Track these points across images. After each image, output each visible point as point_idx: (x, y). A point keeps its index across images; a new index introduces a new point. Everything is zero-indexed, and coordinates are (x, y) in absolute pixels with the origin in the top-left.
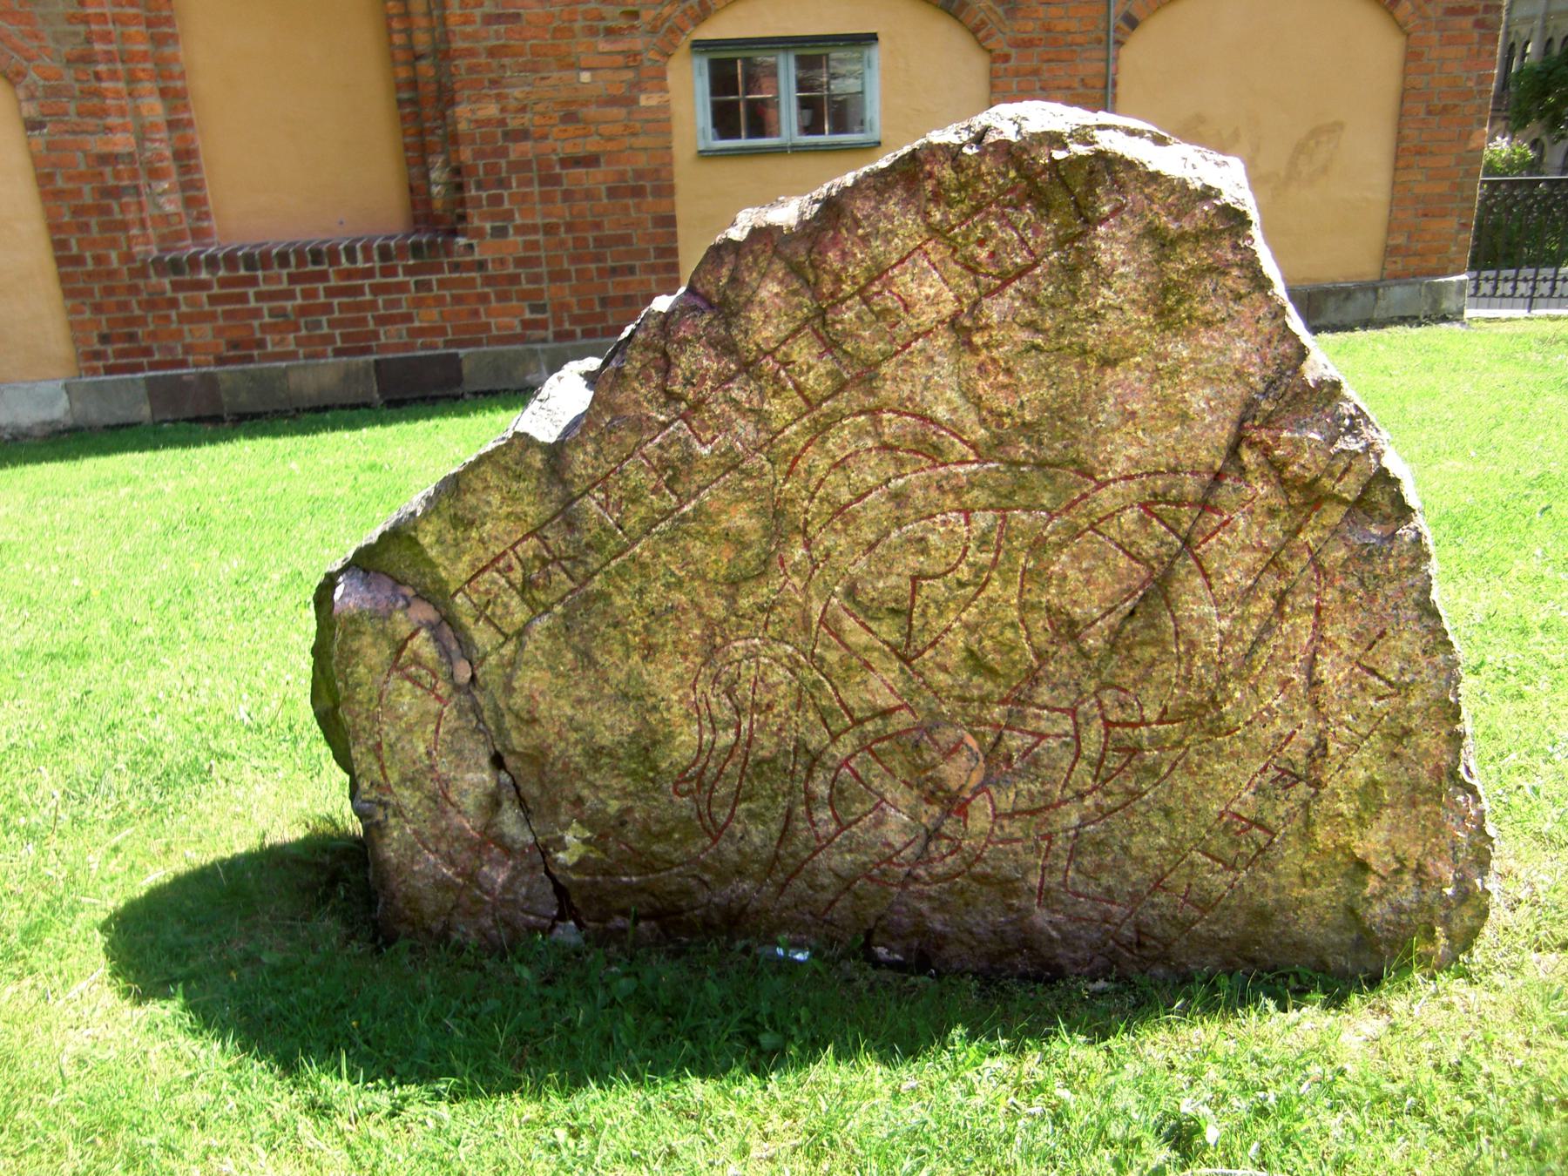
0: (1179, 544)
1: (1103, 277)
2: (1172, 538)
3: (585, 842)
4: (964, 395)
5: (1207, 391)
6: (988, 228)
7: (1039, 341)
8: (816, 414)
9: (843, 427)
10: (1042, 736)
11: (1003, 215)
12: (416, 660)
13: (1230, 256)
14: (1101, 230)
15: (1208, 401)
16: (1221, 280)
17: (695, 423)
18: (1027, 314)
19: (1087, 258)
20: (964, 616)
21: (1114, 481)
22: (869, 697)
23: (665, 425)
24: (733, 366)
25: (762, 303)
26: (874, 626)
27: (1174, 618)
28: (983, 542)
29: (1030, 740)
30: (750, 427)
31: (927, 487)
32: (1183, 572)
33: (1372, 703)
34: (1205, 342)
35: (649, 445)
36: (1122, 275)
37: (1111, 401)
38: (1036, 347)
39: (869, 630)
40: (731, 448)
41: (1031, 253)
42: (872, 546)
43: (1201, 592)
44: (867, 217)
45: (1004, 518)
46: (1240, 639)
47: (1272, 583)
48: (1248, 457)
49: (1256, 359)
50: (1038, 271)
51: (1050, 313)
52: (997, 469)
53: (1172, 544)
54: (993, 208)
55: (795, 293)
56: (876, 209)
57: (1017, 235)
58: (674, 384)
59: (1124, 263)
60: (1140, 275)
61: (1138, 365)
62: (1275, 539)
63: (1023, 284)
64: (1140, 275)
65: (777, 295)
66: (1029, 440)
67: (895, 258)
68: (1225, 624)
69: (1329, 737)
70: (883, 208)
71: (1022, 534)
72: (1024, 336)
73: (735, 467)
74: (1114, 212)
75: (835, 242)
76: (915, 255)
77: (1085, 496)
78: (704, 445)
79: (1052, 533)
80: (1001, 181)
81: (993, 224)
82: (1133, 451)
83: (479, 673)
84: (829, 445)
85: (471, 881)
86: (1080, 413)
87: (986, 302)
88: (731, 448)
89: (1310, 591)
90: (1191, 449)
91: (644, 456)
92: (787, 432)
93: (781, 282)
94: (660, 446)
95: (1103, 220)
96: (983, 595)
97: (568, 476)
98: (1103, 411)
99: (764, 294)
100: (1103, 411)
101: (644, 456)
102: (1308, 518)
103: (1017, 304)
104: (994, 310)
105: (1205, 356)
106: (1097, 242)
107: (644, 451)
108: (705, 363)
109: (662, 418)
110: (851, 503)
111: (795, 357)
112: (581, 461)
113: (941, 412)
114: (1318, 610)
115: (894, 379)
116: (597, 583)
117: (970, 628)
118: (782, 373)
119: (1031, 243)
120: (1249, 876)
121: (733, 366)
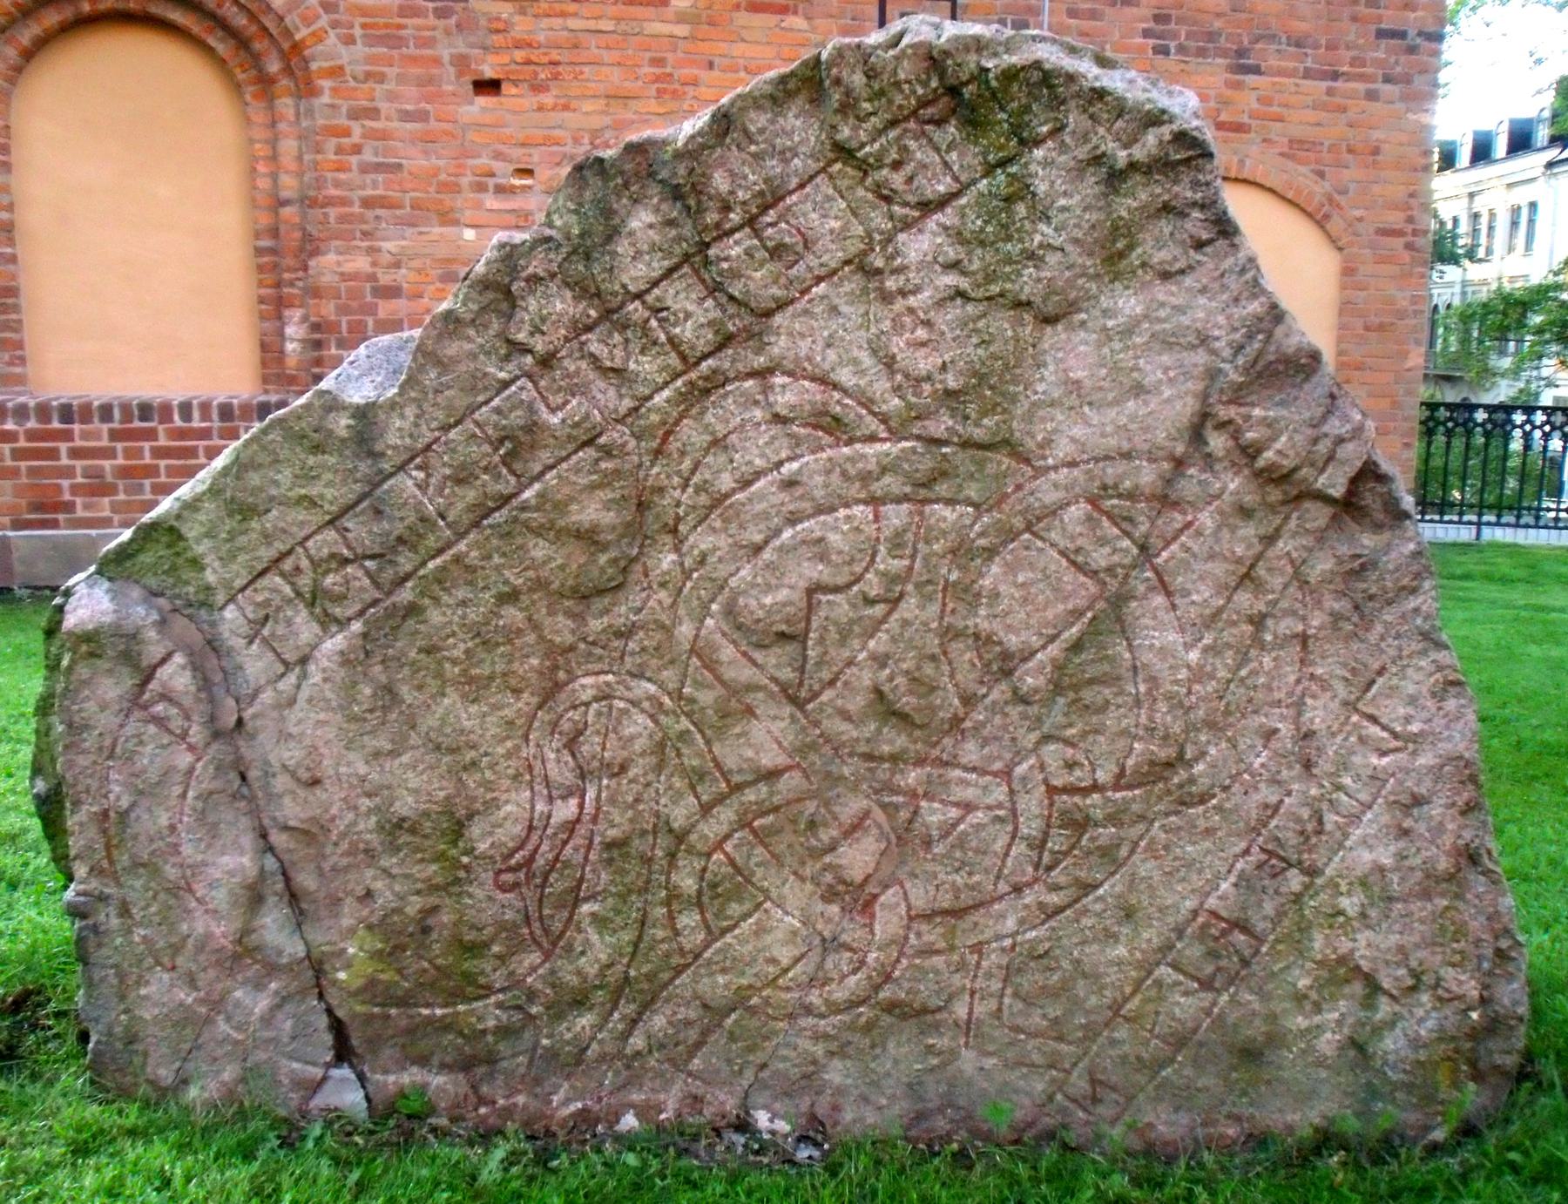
0: (1135, 551)
2: (1126, 543)
4: (874, 352)
7: (964, 283)
8: (693, 375)
10: (968, 807)
12: (165, 697)
13: (1189, 194)
14: (1039, 153)
15: (1166, 370)
18: (951, 253)
19: (1021, 191)
20: (872, 644)
22: (750, 753)
23: (506, 384)
24: (593, 313)
25: (631, 234)
26: (758, 656)
29: (954, 813)
30: (612, 393)
31: (828, 472)
33: (1374, 760)
37: (1051, 368)
39: (754, 663)
40: (587, 416)
42: (758, 549)
44: (762, 131)
45: (921, 513)
48: (1217, 442)
49: (1221, 319)
50: (963, 201)
52: (914, 450)
53: (1126, 551)
55: (671, 223)
56: (772, 122)
57: (941, 160)
60: (1085, 209)
61: (1083, 323)
62: (1249, 547)
63: (947, 217)
64: (1085, 209)
65: (651, 226)
66: (953, 412)
68: (1194, 656)
70: (781, 120)
72: (951, 279)
74: (1054, 133)
75: (722, 163)
76: (818, 180)
77: (1019, 487)
78: (553, 410)
79: (982, 534)
80: (920, 91)
81: (912, 144)
82: (1078, 431)
83: (247, 714)
84: (709, 418)
86: (1015, 381)
87: (902, 237)
88: (587, 416)
91: (477, 423)
92: (657, 399)
93: (657, 210)
94: (498, 411)
95: (1038, 143)
97: (379, 447)
98: (1042, 379)
99: (634, 224)
100: (1042, 379)
101: (477, 423)
104: (918, 246)
105: (1162, 313)
106: (1033, 168)
107: (476, 416)
108: (559, 306)
109: (502, 375)
110: (734, 491)
111: (669, 303)
112: (395, 434)
113: (845, 376)
115: (790, 334)
117: (880, 660)
118: (654, 323)
121: (593, 313)
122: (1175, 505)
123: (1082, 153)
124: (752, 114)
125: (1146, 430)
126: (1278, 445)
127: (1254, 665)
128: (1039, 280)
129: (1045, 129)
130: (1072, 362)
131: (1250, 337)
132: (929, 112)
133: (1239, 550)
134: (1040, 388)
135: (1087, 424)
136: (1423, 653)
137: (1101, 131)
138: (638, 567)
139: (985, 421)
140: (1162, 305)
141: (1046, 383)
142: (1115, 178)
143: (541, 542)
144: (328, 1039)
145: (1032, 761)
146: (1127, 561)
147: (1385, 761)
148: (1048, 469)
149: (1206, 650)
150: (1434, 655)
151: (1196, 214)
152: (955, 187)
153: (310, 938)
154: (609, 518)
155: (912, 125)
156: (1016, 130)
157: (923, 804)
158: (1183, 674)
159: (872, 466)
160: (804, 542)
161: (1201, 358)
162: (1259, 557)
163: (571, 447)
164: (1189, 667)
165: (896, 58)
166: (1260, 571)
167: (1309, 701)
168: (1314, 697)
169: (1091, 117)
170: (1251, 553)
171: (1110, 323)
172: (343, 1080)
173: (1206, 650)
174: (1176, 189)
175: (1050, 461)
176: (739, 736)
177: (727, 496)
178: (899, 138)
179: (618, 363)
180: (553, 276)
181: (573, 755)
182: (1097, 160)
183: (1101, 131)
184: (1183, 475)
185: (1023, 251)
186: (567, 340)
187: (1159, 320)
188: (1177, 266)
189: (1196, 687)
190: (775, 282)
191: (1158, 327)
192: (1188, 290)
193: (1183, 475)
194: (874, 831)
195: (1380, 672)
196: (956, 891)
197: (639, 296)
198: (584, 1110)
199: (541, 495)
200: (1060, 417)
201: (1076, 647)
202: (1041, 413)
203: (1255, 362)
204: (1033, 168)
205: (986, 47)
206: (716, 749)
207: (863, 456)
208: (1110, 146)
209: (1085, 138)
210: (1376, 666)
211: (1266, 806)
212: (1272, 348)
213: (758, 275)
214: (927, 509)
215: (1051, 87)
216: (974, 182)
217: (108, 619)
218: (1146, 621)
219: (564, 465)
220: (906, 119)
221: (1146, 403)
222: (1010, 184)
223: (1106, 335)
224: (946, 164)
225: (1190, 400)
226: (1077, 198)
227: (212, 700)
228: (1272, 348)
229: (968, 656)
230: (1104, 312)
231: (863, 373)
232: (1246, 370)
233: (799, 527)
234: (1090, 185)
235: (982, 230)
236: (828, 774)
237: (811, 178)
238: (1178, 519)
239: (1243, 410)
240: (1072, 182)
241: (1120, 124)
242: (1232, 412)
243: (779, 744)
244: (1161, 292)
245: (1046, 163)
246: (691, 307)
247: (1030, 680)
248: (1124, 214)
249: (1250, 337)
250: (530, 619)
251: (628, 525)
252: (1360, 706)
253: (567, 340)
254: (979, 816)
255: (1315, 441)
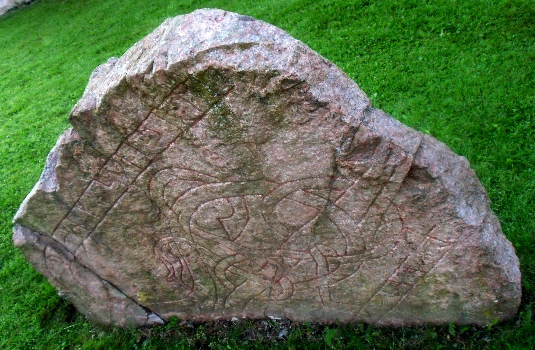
0: (326, 201)
1: (238, 117)
2: (322, 199)
3: (145, 295)
5: (313, 148)
6: (176, 103)
7: (221, 142)
9: (161, 174)
11: (179, 96)
13: (299, 97)
14: (227, 98)
15: (315, 151)
16: (299, 107)
17: (100, 180)
18: (212, 133)
19: (226, 112)
20: (246, 227)
21: (285, 182)
23: (89, 183)
24: (103, 160)
25: (100, 137)
27: (335, 224)
28: (239, 207)
29: (295, 261)
30: (124, 177)
32: (333, 211)
33: (439, 248)
34: (303, 131)
35: (87, 190)
36: (246, 115)
37: (270, 156)
38: (220, 145)
40: (120, 186)
41: (200, 110)
43: (343, 216)
44: (121, 105)
45: (244, 198)
46: (369, 230)
47: (373, 209)
49: (331, 133)
50: (207, 117)
51: (221, 132)
52: (231, 185)
53: (323, 201)
54: (173, 96)
56: (123, 102)
57: (191, 104)
58: (84, 169)
59: (245, 110)
60: (256, 113)
61: (275, 142)
62: (370, 196)
64: (256, 113)
65: (104, 134)
66: (240, 174)
67: (143, 118)
68: (360, 225)
69: (423, 259)
71: (255, 203)
72: (215, 141)
73: (126, 191)
74: (229, 90)
76: (151, 115)
77: (275, 189)
78: (109, 186)
79: (268, 202)
80: (170, 86)
81: (178, 101)
82: (289, 172)
83: (76, 255)
84: (159, 179)
85: (252, 95)
86: (257, 162)
88: (120, 186)
89: (395, 213)
90: (315, 170)
95: (226, 94)
96: (249, 222)
98: (268, 160)
100: (268, 160)
102: (382, 188)
103: (205, 130)
105: (305, 136)
106: (227, 104)
108: (91, 161)
111: (125, 154)
113: (195, 167)
114: (401, 219)
116: (97, 231)
119: (198, 107)
120: (407, 297)
121: (103, 160)
122: (335, 189)
123: (245, 95)
124: (114, 101)
125: (315, 170)
126: (369, 172)
127: (383, 226)
128: (250, 136)
129: (226, 89)
130: (276, 154)
131: (345, 139)
132: (177, 90)
133: (366, 198)
134: (268, 162)
135: (291, 170)
136: (452, 220)
137: (250, 85)
138: (162, 215)
139: (253, 174)
140: (304, 133)
141: (269, 160)
142: (264, 100)
143: (128, 215)
144: (144, 311)
145: (315, 248)
146: (324, 204)
147: (443, 248)
148: (282, 184)
149: (363, 224)
150: (455, 220)
151: (305, 103)
152: (201, 113)
153: (126, 293)
154: (144, 207)
155: (173, 96)
156: (214, 91)
157: (284, 258)
158: (357, 230)
159: (219, 190)
160: (208, 208)
161: (328, 146)
162: (376, 198)
163: (120, 194)
164: (359, 228)
165: (153, 78)
166: (377, 202)
167: (408, 234)
168: (410, 233)
169: (243, 81)
170: (371, 198)
171: (286, 142)
172: (153, 317)
173: (363, 224)
174: (292, 96)
175: (283, 181)
176: (217, 248)
177: (178, 198)
178: (171, 101)
179: (120, 170)
180: (84, 153)
181: (172, 254)
182: (253, 96)
183: (250, 85)
184: (335, 180)
185: (238, 129)
186: (100, 169)
187: (305, 138)
188: (305, 120)
189: (364, 233)
190: (156, 145)
191: (305, 140)
192: (314, 126)
193: (335, 180)
194: (271, 266)
195: (435, 226)
196: (304, 278)
197: (115, 153)
198: (220, 318)
199: (119, 206)
200: (280, 169)
201: (317, 224)
202: (272, 169)
203: (349, 148)
204: (227, 104)
205: (188, 63)
206: (212, 250)
207: (215, 187)
208: (256, 89)
209: (244, 90)
210: (432, 225)
211: (401, 259)
212: (356, 142)
213: (148, 145)
214: (245, 197)
215: (220, 74)
216: (207, 111)
217: (24, 242)
218: (338, 218)
219: (121, 198)
220: (170, 94)
221: (311, 162)
222: (221, 111)
223: (285, 146)
224: (194, 106)
225: (329, 160)
226: (250, 110)
227: (64, 255)
228: (356, 142)
229: (280, 227)
230: (282, 138)
231: (201, 166)
232: (346, 151)
233: (205, 204)
234: (254, 104)
235: (219, 126)
236: (250, 254)
237: (148, 115)
238: (338, 193)
239: (350, 162)
240: (245, 105)
241: (257, 80)
242: (346, 163)
243: (231, 249)
244: (301, 129)
245: (232, 102)
246: (133, 155)
247: (304, 232)
248: (273, 110)
249: (345, 139)
250: (137, 230)
251: (151, 207)
252: (429, 234)
253: (100, 169)
254: (304, 261)
255: (385, 168)
